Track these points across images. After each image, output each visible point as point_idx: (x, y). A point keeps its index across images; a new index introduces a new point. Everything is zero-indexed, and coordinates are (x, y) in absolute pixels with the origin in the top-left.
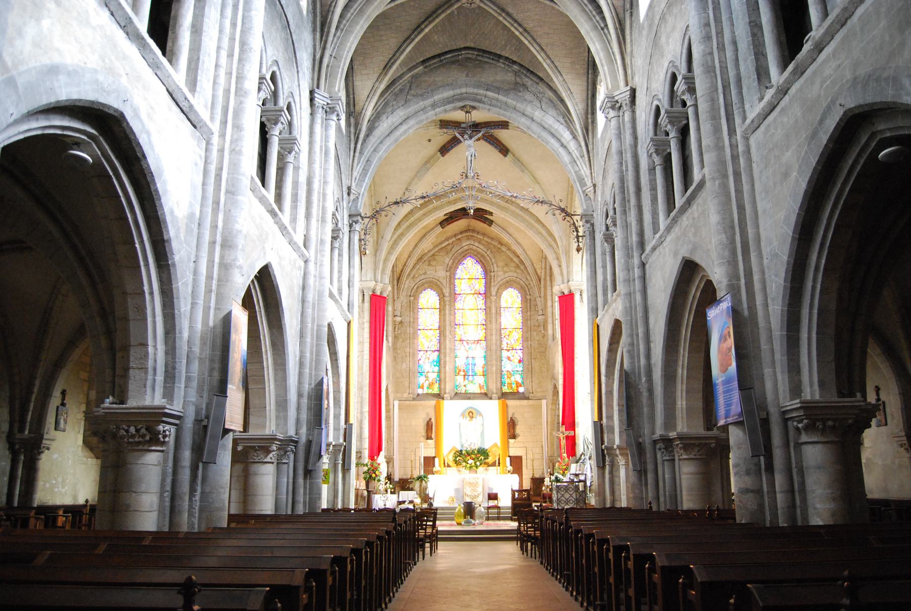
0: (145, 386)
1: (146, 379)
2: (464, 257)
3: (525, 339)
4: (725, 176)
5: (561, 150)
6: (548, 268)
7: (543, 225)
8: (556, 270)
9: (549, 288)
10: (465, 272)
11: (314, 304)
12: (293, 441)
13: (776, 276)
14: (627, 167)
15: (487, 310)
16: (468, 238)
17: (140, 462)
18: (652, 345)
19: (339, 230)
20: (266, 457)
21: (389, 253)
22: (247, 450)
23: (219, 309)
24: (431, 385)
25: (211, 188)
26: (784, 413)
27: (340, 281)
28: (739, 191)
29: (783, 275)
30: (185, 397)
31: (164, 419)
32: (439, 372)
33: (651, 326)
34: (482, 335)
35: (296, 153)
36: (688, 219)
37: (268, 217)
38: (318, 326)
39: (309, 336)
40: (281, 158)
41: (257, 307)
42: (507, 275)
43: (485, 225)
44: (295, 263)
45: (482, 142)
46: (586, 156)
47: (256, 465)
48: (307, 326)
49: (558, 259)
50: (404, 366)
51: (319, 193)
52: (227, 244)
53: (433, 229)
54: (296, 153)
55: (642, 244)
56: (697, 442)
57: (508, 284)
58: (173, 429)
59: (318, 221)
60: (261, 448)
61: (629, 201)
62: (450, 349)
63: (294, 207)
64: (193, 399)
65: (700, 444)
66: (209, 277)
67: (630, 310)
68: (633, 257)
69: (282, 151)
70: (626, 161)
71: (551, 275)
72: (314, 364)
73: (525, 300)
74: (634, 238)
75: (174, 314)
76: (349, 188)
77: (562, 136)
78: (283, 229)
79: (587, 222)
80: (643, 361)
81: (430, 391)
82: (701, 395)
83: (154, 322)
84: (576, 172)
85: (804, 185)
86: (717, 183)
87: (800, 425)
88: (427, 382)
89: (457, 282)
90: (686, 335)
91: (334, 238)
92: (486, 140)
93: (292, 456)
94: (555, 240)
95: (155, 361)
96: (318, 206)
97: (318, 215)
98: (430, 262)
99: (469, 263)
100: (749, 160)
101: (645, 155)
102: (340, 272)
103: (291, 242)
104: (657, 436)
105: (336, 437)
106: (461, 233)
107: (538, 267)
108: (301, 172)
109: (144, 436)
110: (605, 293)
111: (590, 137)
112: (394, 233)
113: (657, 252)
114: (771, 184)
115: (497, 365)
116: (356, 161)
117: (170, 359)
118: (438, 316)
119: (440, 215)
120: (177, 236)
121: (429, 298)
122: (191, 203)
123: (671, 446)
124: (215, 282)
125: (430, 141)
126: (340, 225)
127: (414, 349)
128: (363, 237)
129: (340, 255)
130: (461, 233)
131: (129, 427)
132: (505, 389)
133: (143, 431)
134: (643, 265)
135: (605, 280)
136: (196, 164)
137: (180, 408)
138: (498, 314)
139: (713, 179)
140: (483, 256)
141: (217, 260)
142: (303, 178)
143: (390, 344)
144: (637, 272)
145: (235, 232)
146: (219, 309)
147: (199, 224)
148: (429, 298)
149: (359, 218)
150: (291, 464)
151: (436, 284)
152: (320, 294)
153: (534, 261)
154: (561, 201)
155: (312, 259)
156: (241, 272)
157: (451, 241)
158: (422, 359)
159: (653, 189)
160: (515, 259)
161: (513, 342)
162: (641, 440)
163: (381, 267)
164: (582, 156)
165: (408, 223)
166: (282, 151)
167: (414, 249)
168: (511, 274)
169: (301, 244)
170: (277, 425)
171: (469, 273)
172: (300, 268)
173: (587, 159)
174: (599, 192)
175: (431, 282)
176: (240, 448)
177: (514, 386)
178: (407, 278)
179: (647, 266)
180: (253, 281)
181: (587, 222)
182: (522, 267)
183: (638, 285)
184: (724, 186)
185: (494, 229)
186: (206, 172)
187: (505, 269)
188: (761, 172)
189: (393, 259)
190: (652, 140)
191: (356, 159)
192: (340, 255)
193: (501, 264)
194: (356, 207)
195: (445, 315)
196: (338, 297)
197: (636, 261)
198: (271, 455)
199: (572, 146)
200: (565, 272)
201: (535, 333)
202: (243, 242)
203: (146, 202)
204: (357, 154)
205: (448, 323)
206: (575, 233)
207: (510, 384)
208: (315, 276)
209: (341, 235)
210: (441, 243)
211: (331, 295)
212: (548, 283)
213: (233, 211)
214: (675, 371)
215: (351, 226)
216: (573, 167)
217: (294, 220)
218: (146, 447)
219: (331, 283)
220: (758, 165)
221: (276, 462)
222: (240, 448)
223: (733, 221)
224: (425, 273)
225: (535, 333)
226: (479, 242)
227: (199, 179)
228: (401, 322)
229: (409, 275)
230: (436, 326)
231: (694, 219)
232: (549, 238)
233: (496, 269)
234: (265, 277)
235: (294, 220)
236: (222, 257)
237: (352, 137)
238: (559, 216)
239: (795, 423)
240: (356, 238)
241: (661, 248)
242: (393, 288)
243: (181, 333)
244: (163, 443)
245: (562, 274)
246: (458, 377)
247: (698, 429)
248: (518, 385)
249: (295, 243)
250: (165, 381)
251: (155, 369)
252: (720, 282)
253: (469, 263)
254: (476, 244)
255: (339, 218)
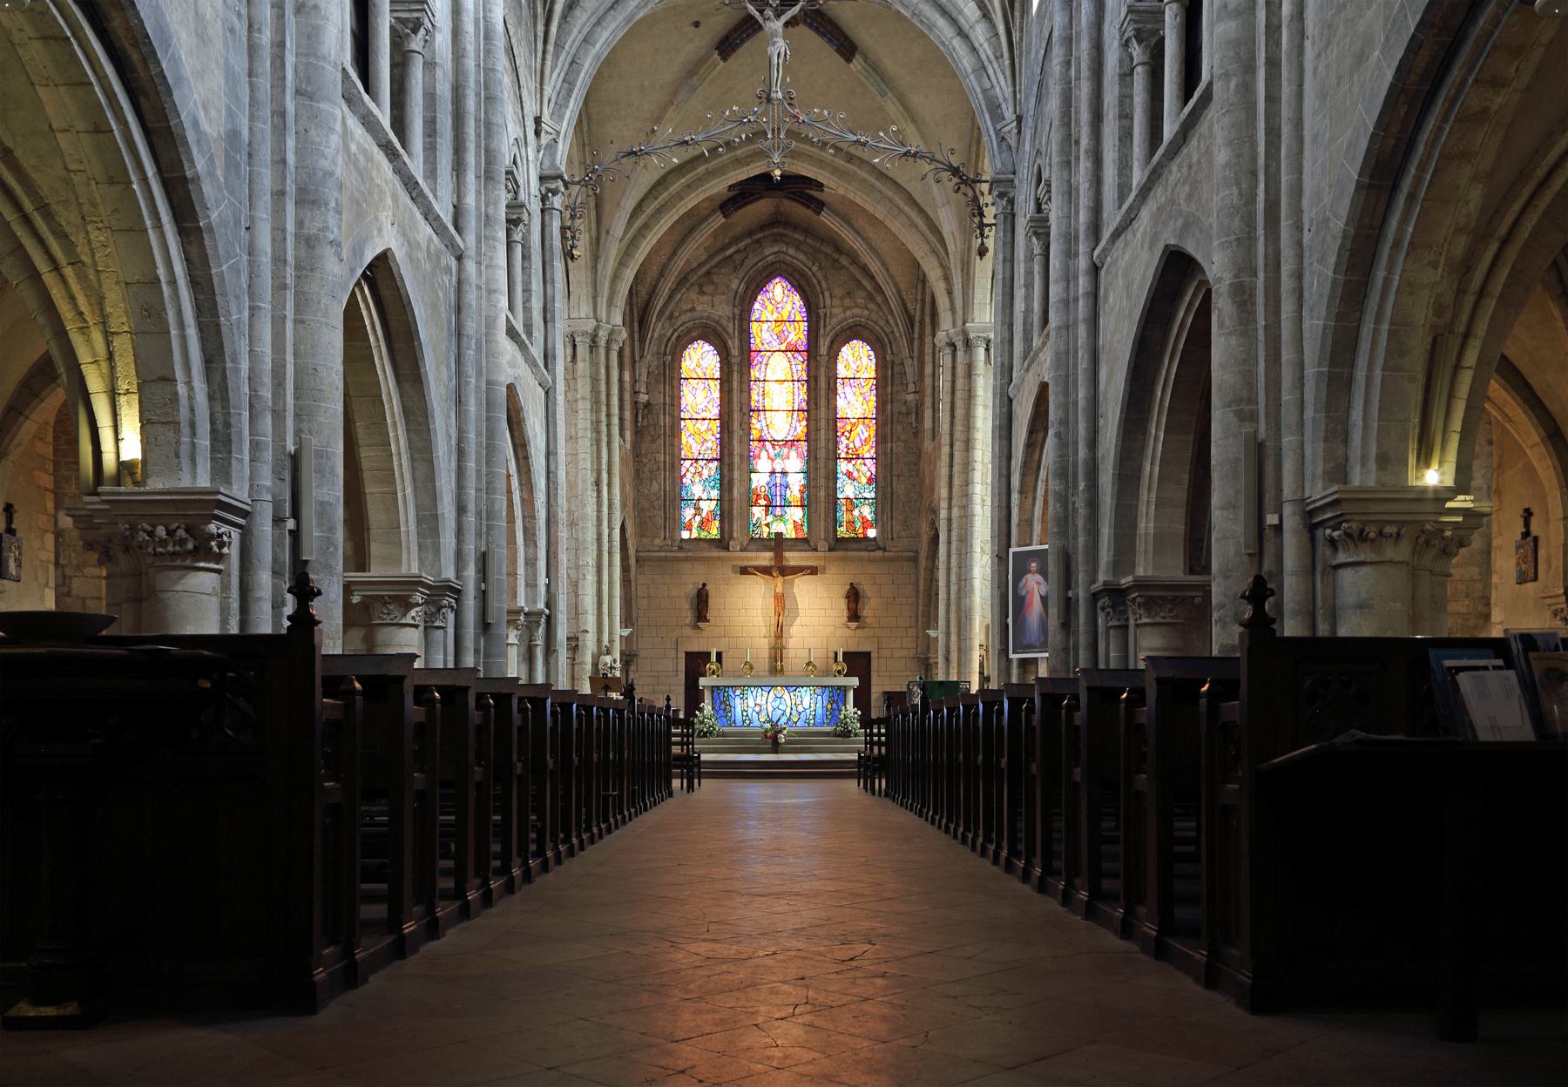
0: (177, 455)
1: (178, 443)
2: (769, 278)
3: (881, 439)
4: (1250, 69)
5: (957, 42)
6: (928, 299)
7: (921, 211)
8: (943, 303)
9: (928, 339)
10: (770, 307)
11: (478, 342)
12: (451, 589)
13: (1322, 260)
14: (1078, 71)
15: (812, 382)
16: (778, 238)
17: (178, 588)
18: (1101, 422)
19: (522, 206)
20: (404, 615)
21: (621, 264)
22: (366, 605)
23: (302, 322)
24: (703, 525)
25: (265, 83)
26: (1311, 514)
27: (527, 310)
28: (1272, 99)
29: (1332, 260)
30: (251, 478)
31: (217, 512)
32: (721, 500)
33: (1102, 387)
34: (801, 429)
35: (427, 31)
36: (1180, 167)
37: (380, 156)
38: (489, 383)
39: (472, 401)
40: (398, 42)
41: (372, 339)
42: (849, 313)
43: (809, 212)
44: (439, 260)
45: (802, 30)
46: (1006, 55)
47: (387, 630)
48: (468, 383)
49: (947, 278)
50: (655, 486)
51: (477, 120)
52: (308, 198)
53: (706, 218)
54: (427, 31)
55: (1095, 229)
56: (1170, 594)
57: (852, 332)
58: (235, 534)
59: (478, 177)
60: (394, 599)
61: (1077, 142)
62: (741, 456)
63: (431, 149)
64: (268, 483)
65: (1176, 598)
66: (279, 260)
67: (1064, 360)
68: (1077, 254)
69: (399, 27)
70: (1078, 59)
71: (934, 314)
72: (484, 452)
73: (881, 365)
74: (1083, 217)
75: (218, 325)
76: (538, 120)
77: (961, 12)
78: (410, 184)
79: (1001, 195)
80: (1082, 453)
81: (703, 535)
82: (1182, 511)
83: (183, 338)
84: (984, 91)
85: (1389, 76)
86: (1233, 85)
87: (1336, 534)
88: (698, 518)
89: (754, 327)
90: (1162, 400)
91: (512, 223)
92: (810, 26)
93: (451, 617)
94: (942, 241)
95: (192, 410)
96: (478, 147)
97: (478, 164)
98: (701, 286)
99: (778, 289)
100: (1300, 34)
101: (1116, 43)
102: (527, 290)
103: (429, 215)
104: (1098, 585)
105: (532, 599)
106: (762, 228)
107: (908, 297)
108: (439, 73)
109: (182, 542)
110: (1027, 338)
111: (1017, 14)
112: (630, 224)
113: (1120, 242)
114: (1334, 80)
115: (827, 488)
116: (549, 62)
117: (218, 408)
118: (717, 395)
119: (719, 186)
120: (211, 174)
121: (701, 359)
122: (229, 109)
123: (1124, 603)
124: (290, 271)
125: (697, 24)
126: (522, 196)
127: (673, 455)
128: (569, 223)
129: (526, 257)
130: (762, 228)
131: (154, 527)
132: (842, 531)
133: (181, 533)
134: (1095, 270)
135: (1028, 311)
136: (232, 30)
137: (245, 496)
138: (832, 392)
139: (1226, 76)
140: (803, 275)
141: (290, 227)
142: (444, 89)
143: (628, 446)
144: (1083, 283)
145: (320, 174)
146: (302, 322)
147: (250, 155)
148: (701, 359)
149: (560, 183)
150: (451, 630)
151: (714, 330)
152: (490, 323)
153: (903, 287)
154: (953, 151)
155: (472, 252)
156: (339, 255)
157: (742, 245)
158: (689, 475)
159: (1125, 116)
160: (866, 283)
161: (858, 444)
162: (1070, 594)
163: (606, 293)
164: (999, 57)
165: (655, 204)
166: (399, 27)
167: (670, 259)
168: (857, 311)
169: (447, 219)
170: (421, 561)
171: (778, 311)
172: (448, 270)
173: (1007, 62)
174: (1027, 134)
175: (705, 326)
176: (356, 599)
177: (858, 524)
178: (658, 319)
179: (1103, 273)
180: (358, 284)
181: (1001, 195)
182: (879, 299)
183: (1082, 308)
184: (1247, 89)
185: (826, 218)
186: (253, 50)
187: (847, 302)
188: (1319, 55)
189: (629, 275)
190: (1130, 10)
191: (549, 57)
192: (526, 257)
193: (838, 292)
194: (553, 161)
195: (730, 391)
196: (524, 337)
197: (1083, 263)
198: (413, 613)
199: (980, 34)
200: (959, 303)
201: (899, 428)
202: (336, 194)
203: (142, 99)
204: (551, 48)
205: (736, 407)
206: (977, 220)
207: (851, 523)
208: (479, 288)
209: (525, 217)
210: (722, 249)
211: (511, 332)
212: (928, 329)
213: (313, 132)
214: (1140, 468)
215: (544, 199)
216: (979, 80)
217: (432, 173)
218: (188, 563)
219: (511, 308)
220: (1313, 44)
221: (422, 624)
222: (356, 599)
223: (1254, 159)
224: (693, 309)
225: (899, 428)
226: (798, 248)
227: (240, 64)
228: (648, 405)
229: (661, 312)
230: (715, 411)
231: (1190, 167)
232: (931, 237)
233: (828, 302)
234: (380, 275)
235: (432, 173)
236: (300, 224)
237: (540, 10)
238: (949, 182)
239: (1328, 531)
240: (556, 225)
241: (1129, 234)
242: (631, 336)
243: (234, 360)
244: (219, 558)
245: (953, 309)
246: (755, 510)
247: (1174, 570)
248: (866, 524)
249: (438, 217)
250: (213, 450)
251: (193, 426)
252: (1220, 280)
253: (778, 289)
254: (791, 251)
255: (521, 182)
